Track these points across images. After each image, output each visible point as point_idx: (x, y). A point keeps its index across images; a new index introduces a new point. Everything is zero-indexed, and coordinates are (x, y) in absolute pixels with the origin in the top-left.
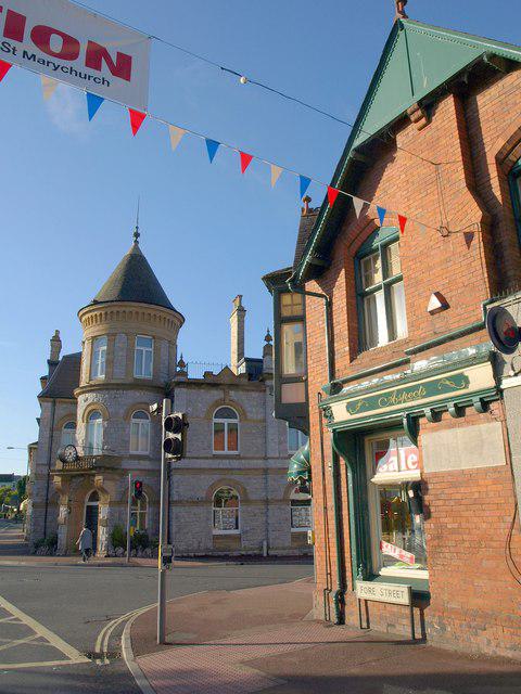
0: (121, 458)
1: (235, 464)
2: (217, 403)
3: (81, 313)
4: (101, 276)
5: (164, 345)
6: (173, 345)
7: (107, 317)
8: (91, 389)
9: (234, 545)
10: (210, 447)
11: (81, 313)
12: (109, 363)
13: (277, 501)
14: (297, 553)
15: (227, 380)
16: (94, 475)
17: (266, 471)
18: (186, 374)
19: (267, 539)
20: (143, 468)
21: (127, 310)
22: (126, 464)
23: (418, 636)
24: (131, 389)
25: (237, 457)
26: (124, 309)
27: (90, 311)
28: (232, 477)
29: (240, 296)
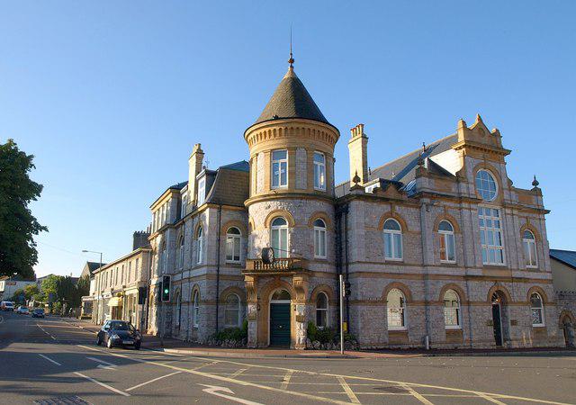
1: (402, 269)
2: (386, 216)
3: (247, 134)
4: (268, 95)
7: (288, 132)
8: (265, 198)
9: (403, 340)
11: (247, 134)
13: (436, 302)
14: (450, 346)
16: (292, 276)
17: (425, 277)
21: (307, 127)
22: (312, 267)
24: (313, 199)
27: (268, 126)
28: (401, 281)
29: (363, 125)
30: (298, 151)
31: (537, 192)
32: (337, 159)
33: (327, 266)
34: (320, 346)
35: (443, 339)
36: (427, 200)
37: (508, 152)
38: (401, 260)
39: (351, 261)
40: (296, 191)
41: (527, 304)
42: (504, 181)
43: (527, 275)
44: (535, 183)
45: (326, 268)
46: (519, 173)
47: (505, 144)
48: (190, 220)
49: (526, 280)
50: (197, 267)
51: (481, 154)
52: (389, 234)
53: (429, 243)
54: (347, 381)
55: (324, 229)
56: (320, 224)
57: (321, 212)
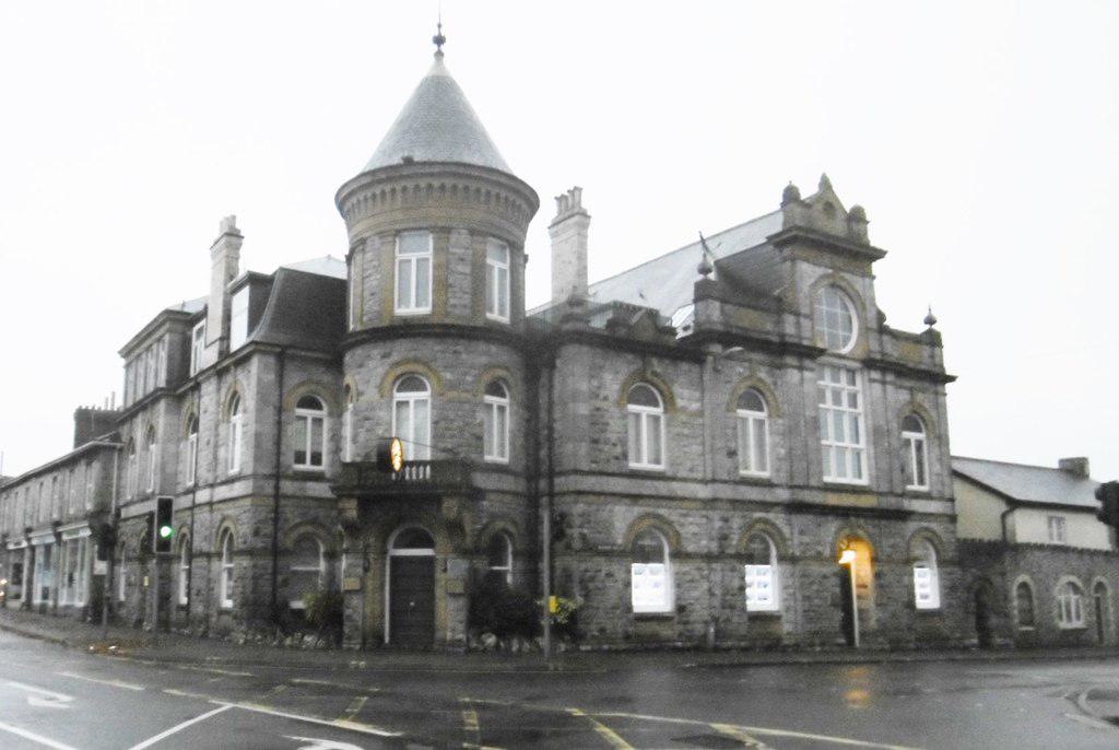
22: (480, 480)
30: (454, 238)
31: (932, 339)
32: (530, 258)
33: (511, 479)
34: (497, 646)
37: (878, 254)
39: (557, 469)
44: (930, 321)
45: (508, 483)
46: (900, 294)
47: (875, 239)
48: (214, 381)
50: (231, 481)
51: (827, 258)
52: (638, 416)
54: (607, 722)
55: (505, 401)
56: (495, 389)
57: (383, 380)
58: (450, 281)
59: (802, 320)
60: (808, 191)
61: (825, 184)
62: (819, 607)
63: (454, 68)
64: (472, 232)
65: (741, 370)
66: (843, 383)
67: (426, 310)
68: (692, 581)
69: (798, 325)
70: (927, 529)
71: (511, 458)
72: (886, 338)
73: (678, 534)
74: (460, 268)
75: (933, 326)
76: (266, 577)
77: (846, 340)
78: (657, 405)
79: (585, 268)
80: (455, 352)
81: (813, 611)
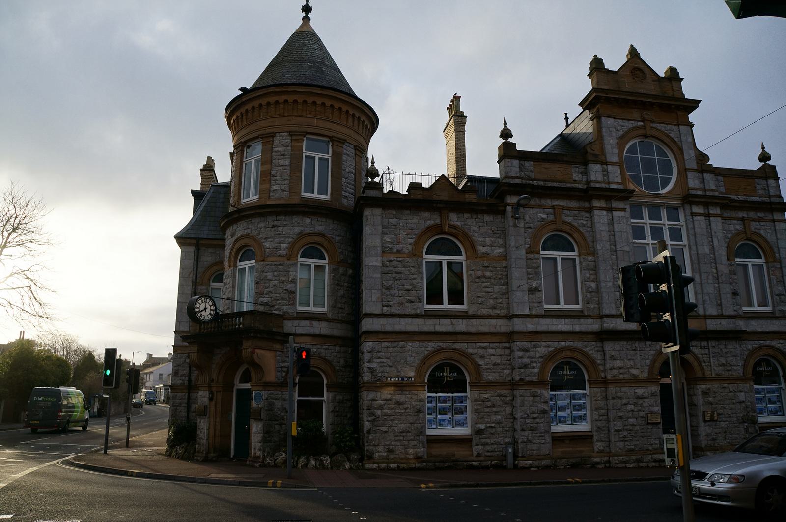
0: (283, 317)
1: (462, 326)
5: (348, 150)
6: (361, 150)
9: (460, 452)
10: (420, 301)
12: (266, 176)
15: (444, 196)
17: (510, 336)
18: (380, 186)
19: (515, 443)
20: (317, 332)
22: (290, 326)
23: (195, 242)
25: (464, 315)
26: (285, 97)
31: (768, 173)
35: (546, 449)
36: (512, 199)
37: (694, 104)
38: (768, 309)
40: (269, 203)
41: (743, 379)
42: (689, 155)
43: (742, 325)
44: (764, 157)
47: (689, 92)
49: (736, 336)
52: (745, 267)
53: (518, 275)
55: (324, 262)
56: (312, 252)
58: (273, 172)
59: (610, 168)
60: (614, 62)
61: (633, 53)
62: (633, 425)
63: (317, 24)
64: (291, 134)
65: (544, 216)
66: (664, 221)
67: (326, 197)
68: (493, 406)
69: (606, 173)
70: (769, 346)
71: (333, 307)
72: (707, 176)
73: (477, 366)
74: (281, 162)
75: (510, 140)
76: (183, 405)
77: (666, 182)
78: (573, 250)
79: (464, 156)
80: (273, 226)
81: (627, 430)
